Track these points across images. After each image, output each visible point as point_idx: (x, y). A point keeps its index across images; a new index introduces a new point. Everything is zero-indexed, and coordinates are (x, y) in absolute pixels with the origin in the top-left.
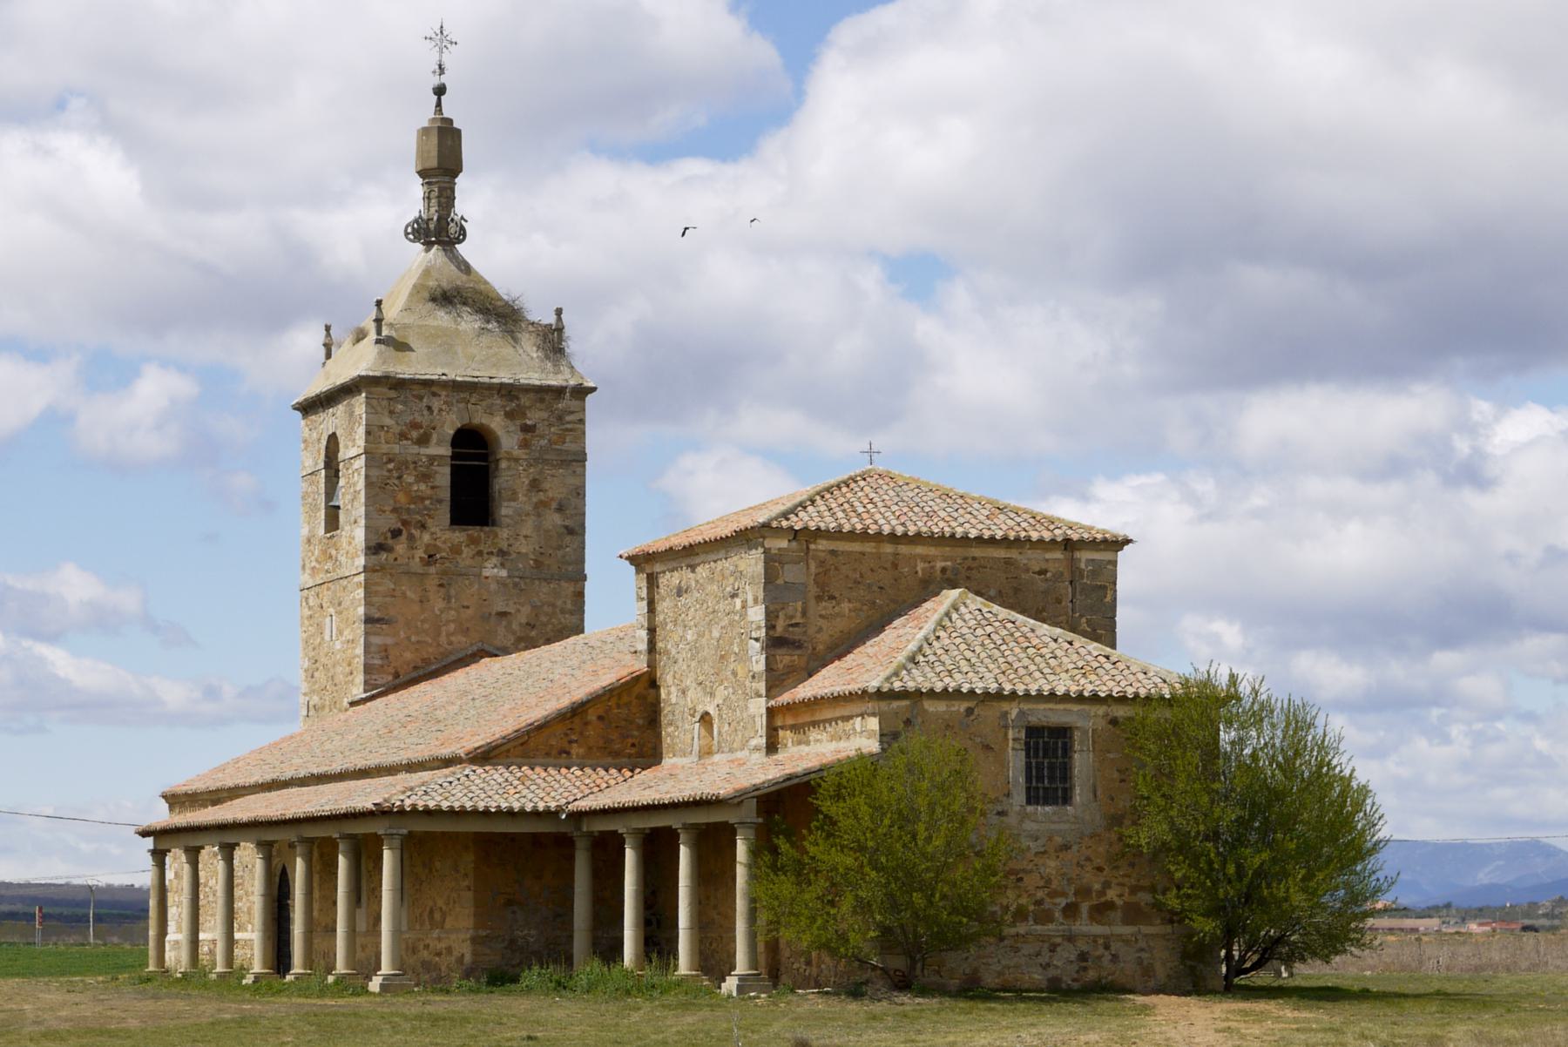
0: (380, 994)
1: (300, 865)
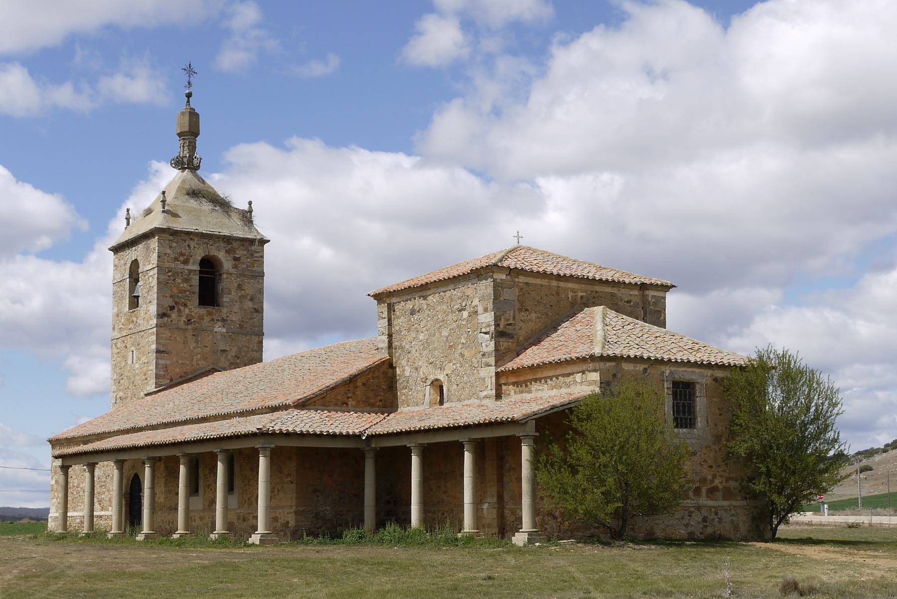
0: (259, 545)
1: (147, 471)
